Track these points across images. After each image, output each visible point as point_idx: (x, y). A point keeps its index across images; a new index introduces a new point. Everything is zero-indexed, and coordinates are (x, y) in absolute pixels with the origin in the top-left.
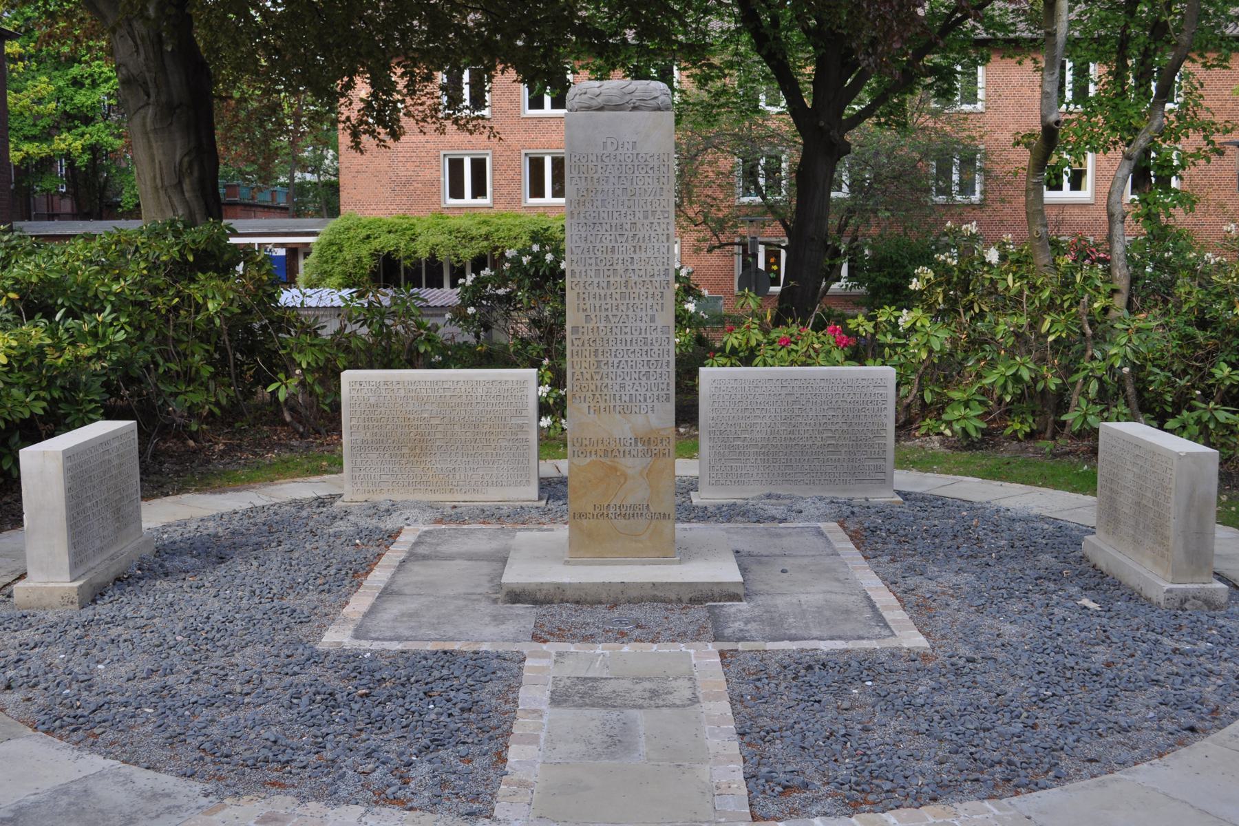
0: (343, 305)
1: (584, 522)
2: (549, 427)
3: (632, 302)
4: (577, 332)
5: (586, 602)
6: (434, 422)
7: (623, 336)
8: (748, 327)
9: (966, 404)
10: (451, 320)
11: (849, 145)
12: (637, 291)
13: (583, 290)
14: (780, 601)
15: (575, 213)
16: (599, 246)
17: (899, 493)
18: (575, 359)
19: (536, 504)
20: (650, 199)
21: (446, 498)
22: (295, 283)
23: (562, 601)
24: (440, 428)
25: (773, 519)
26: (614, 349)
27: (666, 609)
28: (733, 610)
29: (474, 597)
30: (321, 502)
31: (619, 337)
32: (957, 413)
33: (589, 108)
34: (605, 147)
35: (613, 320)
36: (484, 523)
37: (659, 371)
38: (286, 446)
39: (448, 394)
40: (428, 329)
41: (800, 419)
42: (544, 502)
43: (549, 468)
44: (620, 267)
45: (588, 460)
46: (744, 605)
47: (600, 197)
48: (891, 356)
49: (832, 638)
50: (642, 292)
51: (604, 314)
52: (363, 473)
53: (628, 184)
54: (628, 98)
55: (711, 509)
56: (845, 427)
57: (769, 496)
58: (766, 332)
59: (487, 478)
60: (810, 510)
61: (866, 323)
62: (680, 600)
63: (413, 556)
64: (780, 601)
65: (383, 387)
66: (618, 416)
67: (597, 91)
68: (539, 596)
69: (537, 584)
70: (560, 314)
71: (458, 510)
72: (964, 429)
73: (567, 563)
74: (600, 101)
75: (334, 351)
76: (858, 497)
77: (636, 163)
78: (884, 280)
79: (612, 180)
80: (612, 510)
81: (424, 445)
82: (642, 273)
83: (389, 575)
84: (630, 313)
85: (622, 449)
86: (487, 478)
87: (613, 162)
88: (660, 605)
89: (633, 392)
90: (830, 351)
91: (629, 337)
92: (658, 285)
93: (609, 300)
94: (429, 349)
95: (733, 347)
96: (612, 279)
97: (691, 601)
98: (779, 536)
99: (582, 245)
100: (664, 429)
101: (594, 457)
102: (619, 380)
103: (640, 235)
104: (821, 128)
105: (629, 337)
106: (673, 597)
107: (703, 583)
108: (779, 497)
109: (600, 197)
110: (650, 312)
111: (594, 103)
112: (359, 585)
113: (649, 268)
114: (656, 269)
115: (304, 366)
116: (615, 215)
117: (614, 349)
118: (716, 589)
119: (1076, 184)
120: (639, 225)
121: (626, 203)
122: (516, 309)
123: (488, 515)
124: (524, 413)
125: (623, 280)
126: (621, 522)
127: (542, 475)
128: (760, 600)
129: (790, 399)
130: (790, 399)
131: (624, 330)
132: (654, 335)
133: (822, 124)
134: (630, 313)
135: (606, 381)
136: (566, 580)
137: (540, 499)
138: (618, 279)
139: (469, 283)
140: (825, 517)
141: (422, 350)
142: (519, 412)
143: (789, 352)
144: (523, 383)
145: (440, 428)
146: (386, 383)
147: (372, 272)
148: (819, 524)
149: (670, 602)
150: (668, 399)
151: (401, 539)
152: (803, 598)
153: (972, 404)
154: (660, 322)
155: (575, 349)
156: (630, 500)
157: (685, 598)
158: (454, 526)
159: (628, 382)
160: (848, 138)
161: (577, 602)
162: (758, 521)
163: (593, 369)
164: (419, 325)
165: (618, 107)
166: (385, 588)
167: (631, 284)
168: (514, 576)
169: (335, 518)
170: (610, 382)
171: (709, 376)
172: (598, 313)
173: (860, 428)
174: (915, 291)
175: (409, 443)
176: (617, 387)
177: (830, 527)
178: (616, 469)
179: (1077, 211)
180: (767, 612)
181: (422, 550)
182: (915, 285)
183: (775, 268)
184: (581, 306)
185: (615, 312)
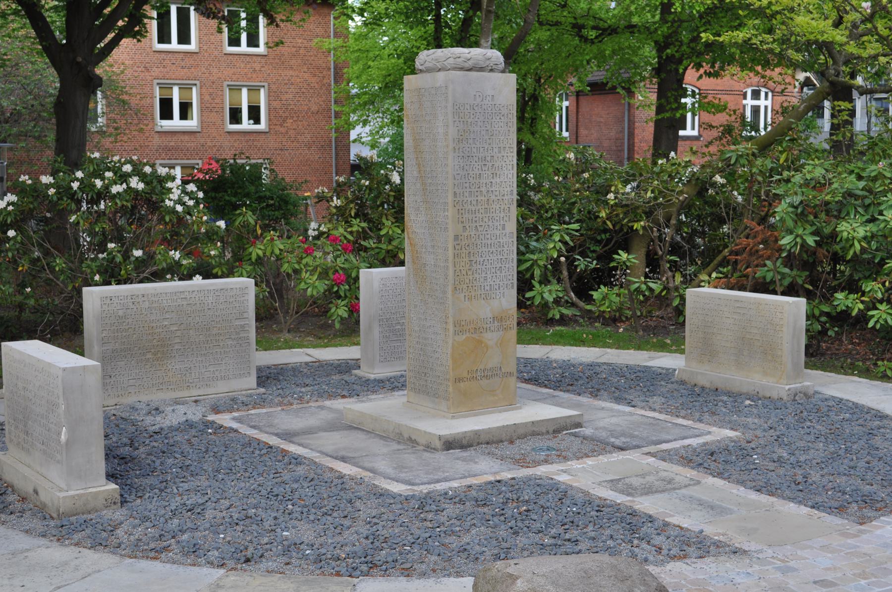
1: (462, 385)
11: (100, 79)
12: (494, 206)
15: (457, 148)
16: (471, 173)
20: (502, 138)
23: (478, 444)
33: (462, 69)
34: (475, 99)
37: (507, 266)
44: (483, 189)
47: (472, 136)
49: (429, 483)
53: (489, 127)
54: (488, 62)
66: (483, 302)
67: (469, 56)
68: (465, 442)
74: (470, 64)
77: (494, 111)
79: (479, 123)
80: (479, 374)
82: (497, 193)
84: (490, 223)
86: (217, 373)
87: (480, 110)
89: (492, 283)
92: (506, 202)
95: (259, 257)
96: (479, 198)
99: (461, 173)
102: (483, 275)
103: (496, 165)
104: (78, 63)
106: (544, 431)
109: (472, 136)
110: (502, 222)
111: (467, 65)
113: (501, 189)
114: (506, 190)
116: (482, 149)
119: (184, 116)
120: (495, 158)
121: (488, 141)
124: (245, 315)
125: (486, 199)
126: (485, 382)
133: (79, 59)
135: (476, 276)
138: (483, 198)
142: (241, 316)
144: (244, 289)
156: (489, 366)
157: (551, 431)
159: (489, 276)
160: (98, 71)
161: (488, 443)
165: (481, 69)
167: (491, 202)
176: (482, 280)
178: (481, 342)
179: (186, 138)
184: (461, 219)
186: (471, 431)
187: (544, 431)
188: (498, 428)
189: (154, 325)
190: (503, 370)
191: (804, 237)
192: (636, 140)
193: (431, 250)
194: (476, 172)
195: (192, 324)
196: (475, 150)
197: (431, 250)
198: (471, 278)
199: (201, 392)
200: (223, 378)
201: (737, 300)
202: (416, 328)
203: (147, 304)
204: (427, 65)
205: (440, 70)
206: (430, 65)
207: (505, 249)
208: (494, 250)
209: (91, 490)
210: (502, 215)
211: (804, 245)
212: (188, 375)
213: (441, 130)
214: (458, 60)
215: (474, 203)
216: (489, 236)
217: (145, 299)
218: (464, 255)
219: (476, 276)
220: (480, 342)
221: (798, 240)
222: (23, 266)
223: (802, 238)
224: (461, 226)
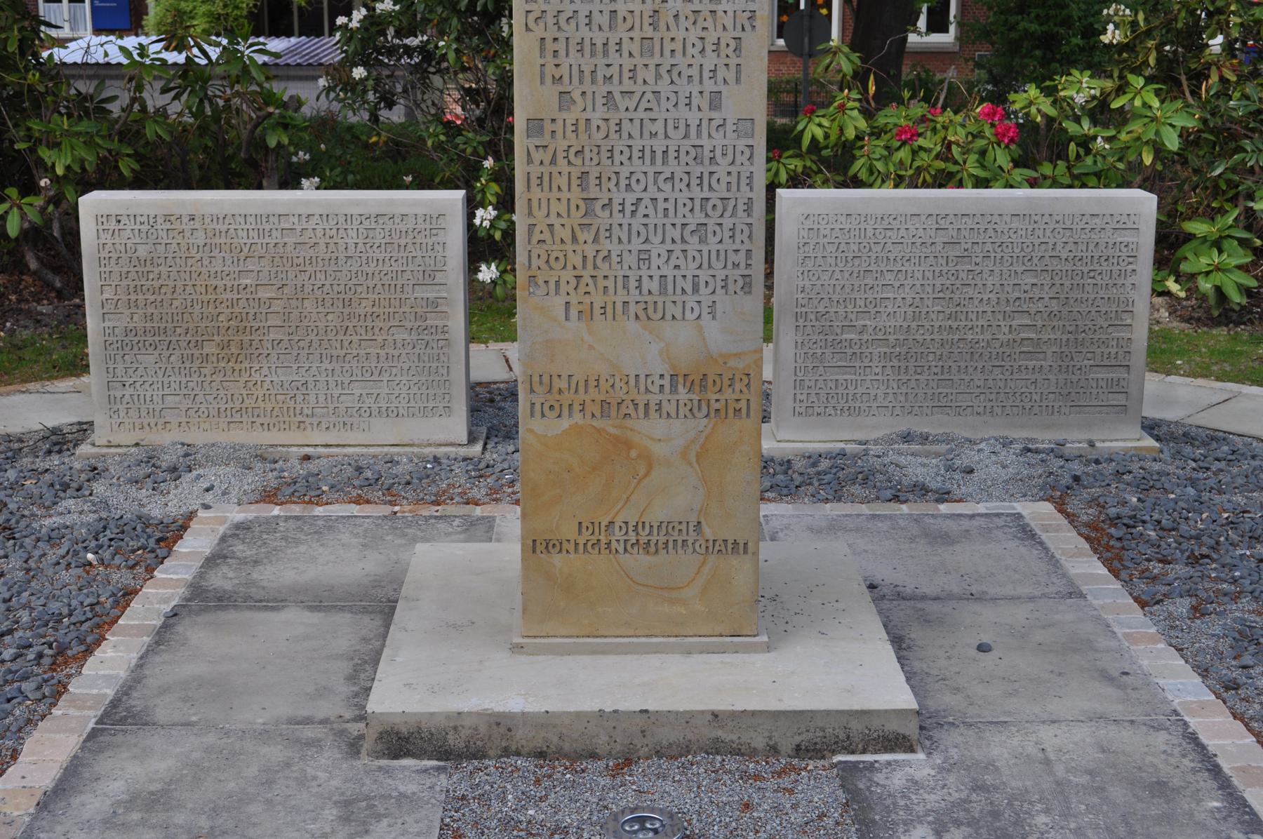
0: (125, 61)
1: (557, 560)
2: (493, 282)
3: (668, 61)
4: (541, 131)
5: (560, 754)
6: (264, 294)
7: (647, 142)
8: (842, 107)
9: (1218, 245)
10: (329, 90)
12: (680, 35)
13: (552, 32)
14: (1000, 748)
17: (1151, 427)
18: (536, 193)
19: (463, 452)
21: (290, 440)
22: (142, 27)
23: (506, 752)
24: (277, 306)
25: (921, 491)
26: (624, 172)
27: (745, 776)
28: (897, 781)
29: (308, 732)
30: (57, 442)
31: (637, 143)
32: (1204, 260)
35: (622, 103)
36: (358, 501)
37: (727, 222)
38: (29, 314)
39: (290, 240)
40: (285, 106)
41: (970, 292)
42: (478, 448)
43: (489, 362)
45: (565, 423)
46: (918, 764)
48: (1078, 156)
50: (692, 37)
51: (602, 89)
52: (129, 391)
55: (799, 465)
56: (1054, 306)
57: (907, 438)
58: (868, 114)
59: (369, 402)
60: (989, 469)
61: (1042, 99)
62: (774, 750)
63: (201, 599)
64: (1000, 748)
65: (162, 226)
66: (632, 325)
69: (448, 716)
70: (506, 80)
71: (312, 466)
72: (1218, 290)
73: (517, 649)
75: (115, 145)
76: (1076, 439)
78: (1034, 27)
80: (618, 535)
81: (246, 339)
83: (134, 657)
84: (664, 86)
85: (641, 399)
88: (732, 764)
89: (668, 271)
90: (983, 153)
91: (659, 145)
92: (728, 22)
93: (613, 58)
94: (285, 141)
97: (798, 751)
98: (945, 539)
100: (737, 355)
101: (577, 417)
102: (637, 244)
105: (659, 145)
106: (759, 742)
107: (828, 713)
108: (925, 438)
110: (709, 86)
112: (60, 690)
115: (60, 171)
117: (624, 172)
118: (856, 726)
122: (439, 71)
123: (369, 481)
126: (638, 561)
127: (476, 376)
128: (953, 742)
129: (953, 252)
130: (953, 252)
131: (649, 127)
132: (719, 140)
134: (664, 86)
135: (606, 245)
136: (513, 702)
137: (472, 439)
139: (354, 24)
140: (1019, 487)
141: (272, 143)
142: (429, 277)
143: (914, 153)
144: (435, 219)
145: (277, 306)
146: (167, 218)
147: (250, 13)
148: (1020, 507)
149: (752, 753)
150: (747, 287)
151: (182, 547)
152: (1048, 735)
153: (1226, 244)
154: (731, 109)
155: (535, 170)
156: (658, 514)
157: (787, 745)
158: (296, 510)
159: (656, 248)
161: (541, 755)
162: (896, 498)
163: (577, 216)
164: (269, 98)
166: (115, 703)
167: (666, 17)
168: (396, 695)
169: (65, 487)
170: (615, 249)
171: (781, 193)
172: (587, 87)
173: (1084, 308)
174: (1111, 45)
175: (213, 333)
176: (630, 260)
177: (1039, 512)
178: (628, 445)
180: (978, 788)
181: (222, 579)
182: (1112, 35)
183: (824, 11)
184: (550, 69)
185: (628, 85)
186: (479, 714)
187: (759, 742)
188: (578, 715)
189: (220, 283)
190: (708, 532)
195: (308, 289)
198: (590, 251)
199: (318, 437)
200: (386, 413)
203: (200, 238)
207: (721, 171)
208: (679, 172)
209: (1107, 444)
210: (710, 61)
212: (299, 398)
215: (605, 20)
217: (197, 224)
218: (563, 182)
222: (378, 134)
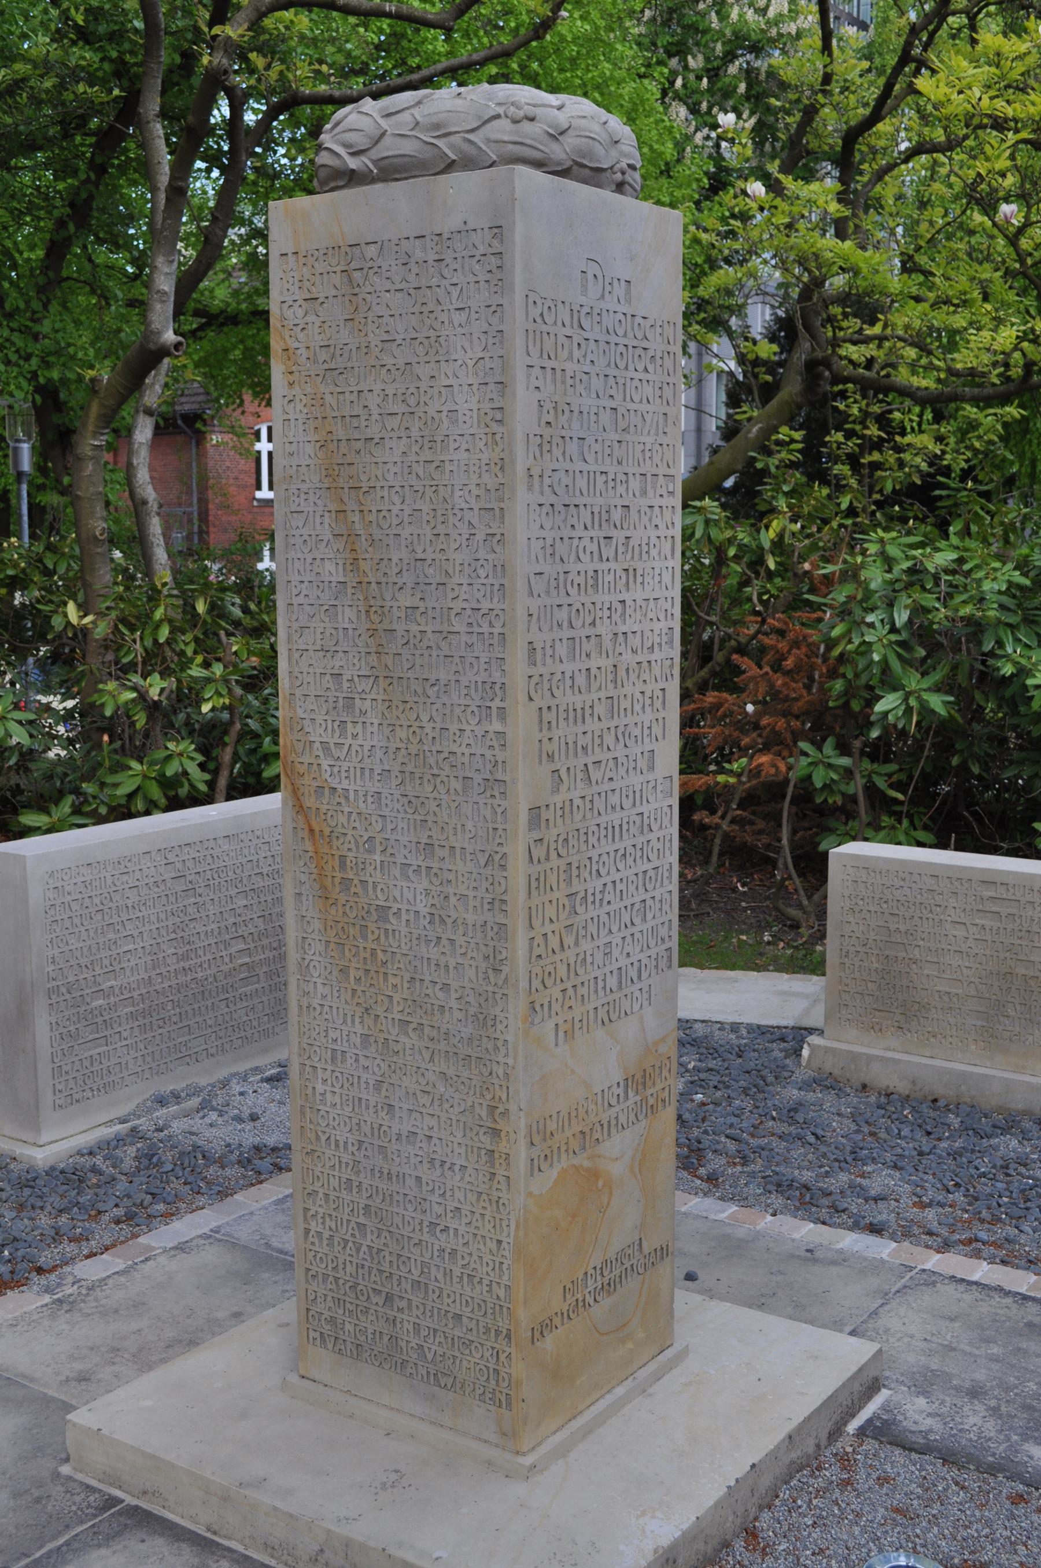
67: (562, 118)
111: (558, 152)
125: (611, 661)
191: (925, 696)
192: (211, 506)
193: (415, 861)
194: (588, 565)
196: (582, 483)
197: (415, 861)
201: (989, 880)
202: (342, 1134)
204: (389, 148)
205: (450, 167)
206: (408, 147)
211: (926, 710)
213: (468, 403)
214: (526, 126)
216: (615, 799)
219: (586, 945)
220: (594, 1174)
221: (912, 702)
223: (919, 698)
224: (547, 768)
